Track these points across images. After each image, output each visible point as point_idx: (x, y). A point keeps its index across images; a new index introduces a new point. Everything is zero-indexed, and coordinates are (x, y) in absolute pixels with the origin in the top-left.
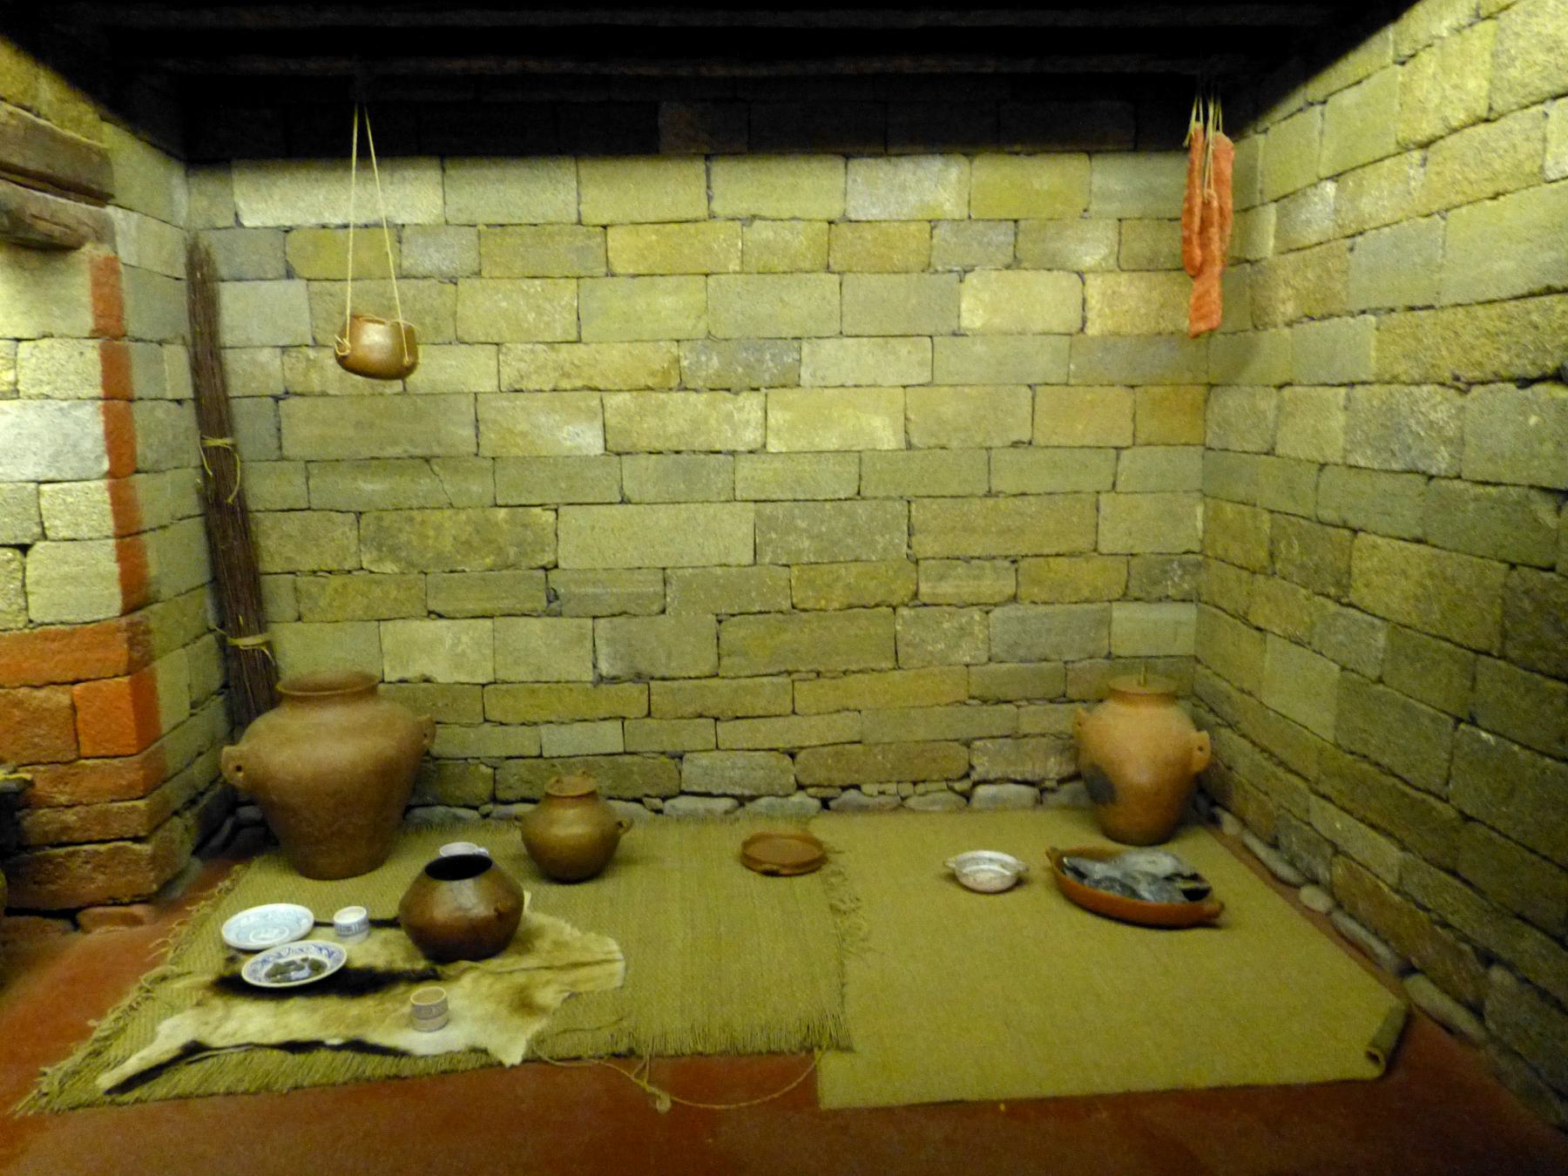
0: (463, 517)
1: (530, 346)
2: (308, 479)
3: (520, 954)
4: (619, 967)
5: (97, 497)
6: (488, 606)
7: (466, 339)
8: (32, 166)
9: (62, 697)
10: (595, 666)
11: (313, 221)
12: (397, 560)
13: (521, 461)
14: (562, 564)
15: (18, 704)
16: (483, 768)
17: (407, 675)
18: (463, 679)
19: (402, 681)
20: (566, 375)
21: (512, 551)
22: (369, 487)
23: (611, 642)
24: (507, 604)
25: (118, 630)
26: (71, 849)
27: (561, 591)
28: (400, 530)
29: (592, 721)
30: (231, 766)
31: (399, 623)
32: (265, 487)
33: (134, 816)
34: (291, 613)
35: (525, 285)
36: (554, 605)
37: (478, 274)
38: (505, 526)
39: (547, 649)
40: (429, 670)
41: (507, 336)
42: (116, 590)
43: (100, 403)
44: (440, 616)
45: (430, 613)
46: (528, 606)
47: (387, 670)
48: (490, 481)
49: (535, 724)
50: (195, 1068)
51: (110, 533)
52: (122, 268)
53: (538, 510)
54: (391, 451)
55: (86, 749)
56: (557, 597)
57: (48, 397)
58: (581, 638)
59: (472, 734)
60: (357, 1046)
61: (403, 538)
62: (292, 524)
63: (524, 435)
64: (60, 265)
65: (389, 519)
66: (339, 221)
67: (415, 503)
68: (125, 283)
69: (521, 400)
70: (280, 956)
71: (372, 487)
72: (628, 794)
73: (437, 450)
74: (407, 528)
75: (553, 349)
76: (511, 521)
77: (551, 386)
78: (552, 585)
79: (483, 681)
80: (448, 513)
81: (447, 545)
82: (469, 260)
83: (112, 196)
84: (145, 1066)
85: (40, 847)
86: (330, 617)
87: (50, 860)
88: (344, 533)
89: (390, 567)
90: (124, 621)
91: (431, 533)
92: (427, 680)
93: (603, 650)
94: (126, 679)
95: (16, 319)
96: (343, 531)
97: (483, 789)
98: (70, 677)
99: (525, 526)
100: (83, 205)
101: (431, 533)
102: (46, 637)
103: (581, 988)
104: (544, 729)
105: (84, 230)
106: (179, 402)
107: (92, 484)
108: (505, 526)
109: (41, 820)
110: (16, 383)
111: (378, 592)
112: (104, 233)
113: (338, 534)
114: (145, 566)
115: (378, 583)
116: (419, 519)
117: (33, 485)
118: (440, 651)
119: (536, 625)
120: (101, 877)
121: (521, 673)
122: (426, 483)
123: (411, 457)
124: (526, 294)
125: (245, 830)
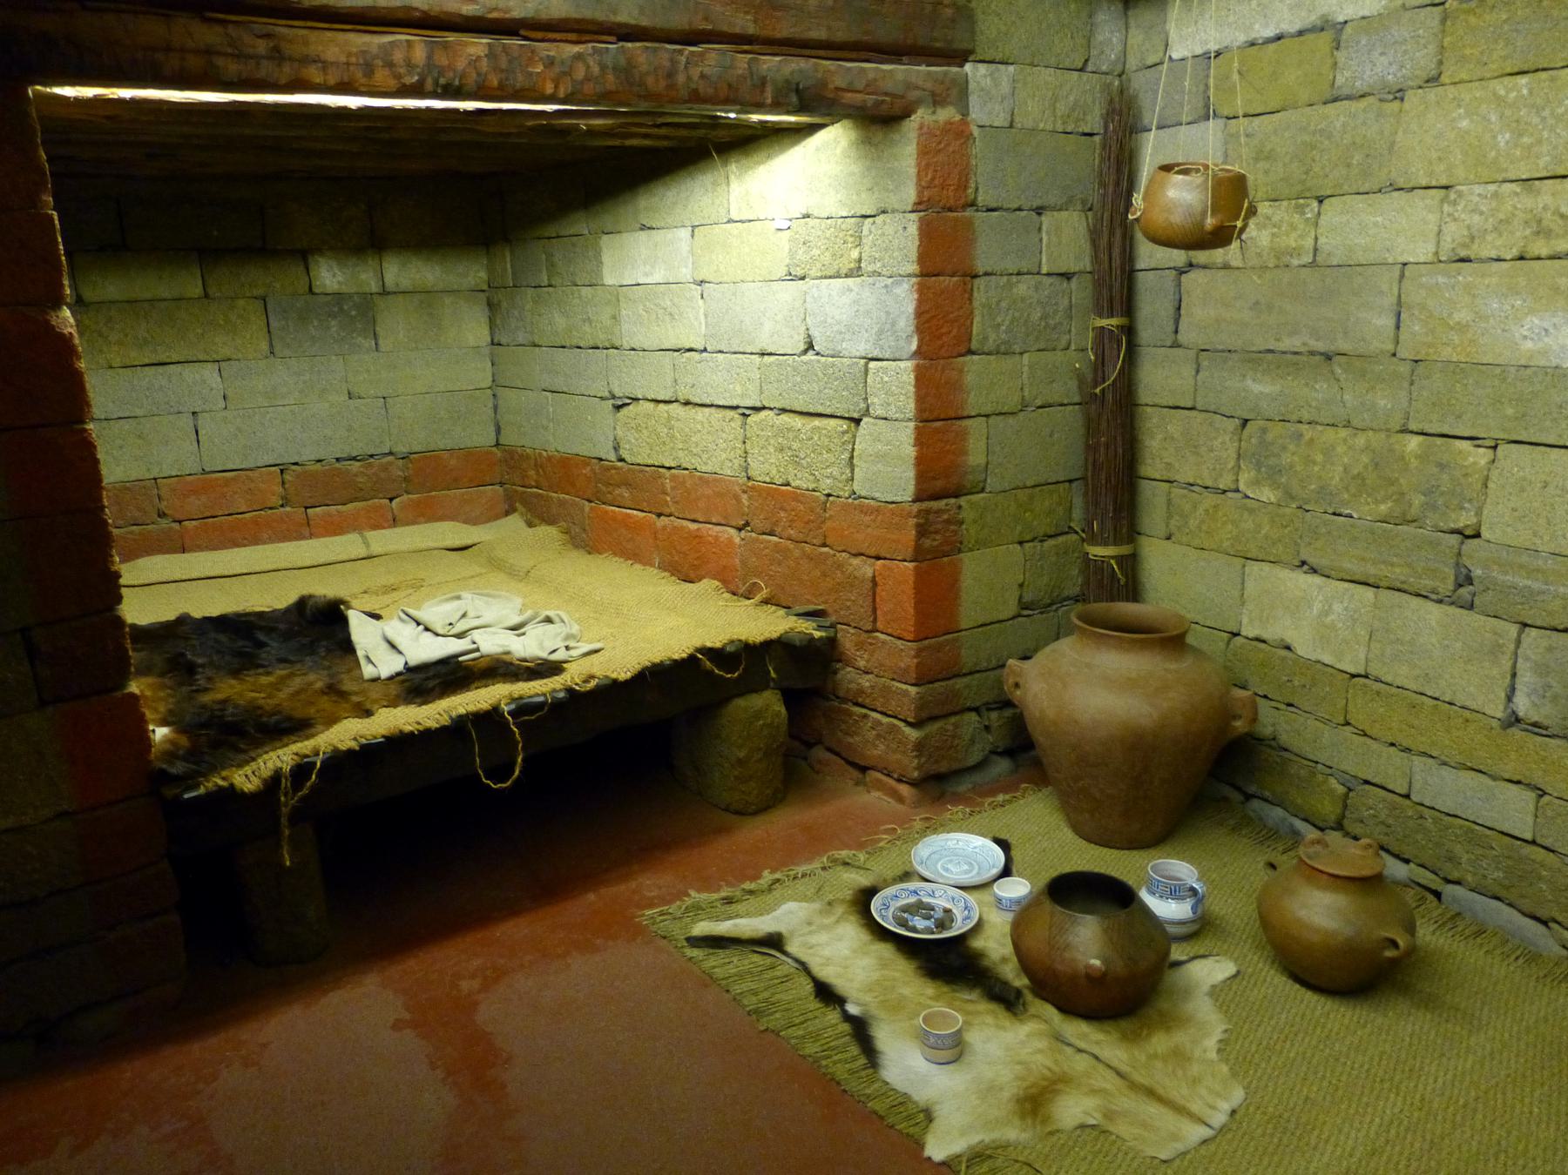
0: (1361, 440)
1: (1492, 188)
2: (1198, 372)
3: (1168, 1029)
4: (1198, 1133)
5: (905, 377)
6: (1372, 571)
7: (1401, 182)
8: (840, 36)
9: (866, 569)
10: (1509, 699)
11: (1242, 38)
12: (1275, 486)
13: (1455, 369)
14: (1485, 534)
15: (840, 566)
16: (1333, 782)
17: (1265, 636)
18: (1327, 659)
19: (1258, 639)
20: (1542, 232)
21: (1418, 500)
22: (1257, 388)
23: (1542, 670)
24: (1398, 573)
25: (909, 515)
26: (864, 711)
27: (1477, 572)
28: (1284, 448)
29: (1494, 778)
30: (1011, 681)
31: (1266, 567)
32: (1160, 377)
33: (905, 700)
34: (1163, 532)
35: (1500, 87)
36: (1463, 590)
37: (1433, 80)
38: (1414, 463)
39: (1437, 648)
40: (1290, 636)
41: (1460, 173)
42: (910, 474)
43: (914, 280)
44: (1314, 571)
45: (1304, 563)
46: (1426, 583)
47: (1245, 621)
48: (1403, 394)
49: (1407, 750)
50: (756, 958)
51: (911, 415)
52: (976, 131)
53: (1466, 445)
54: (1287, 344)
55: (880, 625)
56: (1469, 580)
57: (880, 275)
58: (1495, 650)
59: (1327, 734)
60: (860, 1029)
61: (1286, 459)
62: (1175, 424)
63: (1462, 328)
64: (896, 137)
65: (1276, 431)
66: (1270, 32)
67: (1306, 417)
68: (977, 149)
69: (1466, 273)
70: (932, 895)
71: (1261, 388)
72: (1526, 905)
73: (1343, 345)
74: (1292, 447)
75: (1530, 190)
76: (1423, 457)
77: (1515, 252)
78: (1466, 561)
79: (1352, 670)
80: (1343, 433)
81: (1336, 477)
82: (1424, 60)
83: (971, 52)
84: (733, 934)
85: (845, 700)
86: (1196, 542)
87: (850, 714)
88: (1223, 443)
89: (1267, 494)
90: (916, 507)
91: (1319, 458)
92: (1288, 648)
93: (1526, 678)
94: (911, 565)
95: (863, 196)
96: (1223, 443)
97: (1329, 810)
98: (872, 552)
99: (1442, 466)
100: (923, 68)
101: (1319, 458)
102: (864, 510)
103: (1122, 1129)
104: (1418, 761)
105: (914, 95)
106: (1067, 276)
107: (902, 364)
108: (1414, 463)
109: (849, 678)
110: (860, 260)
111: (1248, 524)
112: (959, 94)
113: (1216, 443)
114: (964, 453)
115: (1251, 511)
116: (1307, 437)
117: (863, 362)
118: (1305, 616)
119: (1434, 613)
120: (882, 747)
121: (1401, 674)
122: (1321, 390)
123: (1312, 353)
124: (1499, 101)
125: (984, 749)
